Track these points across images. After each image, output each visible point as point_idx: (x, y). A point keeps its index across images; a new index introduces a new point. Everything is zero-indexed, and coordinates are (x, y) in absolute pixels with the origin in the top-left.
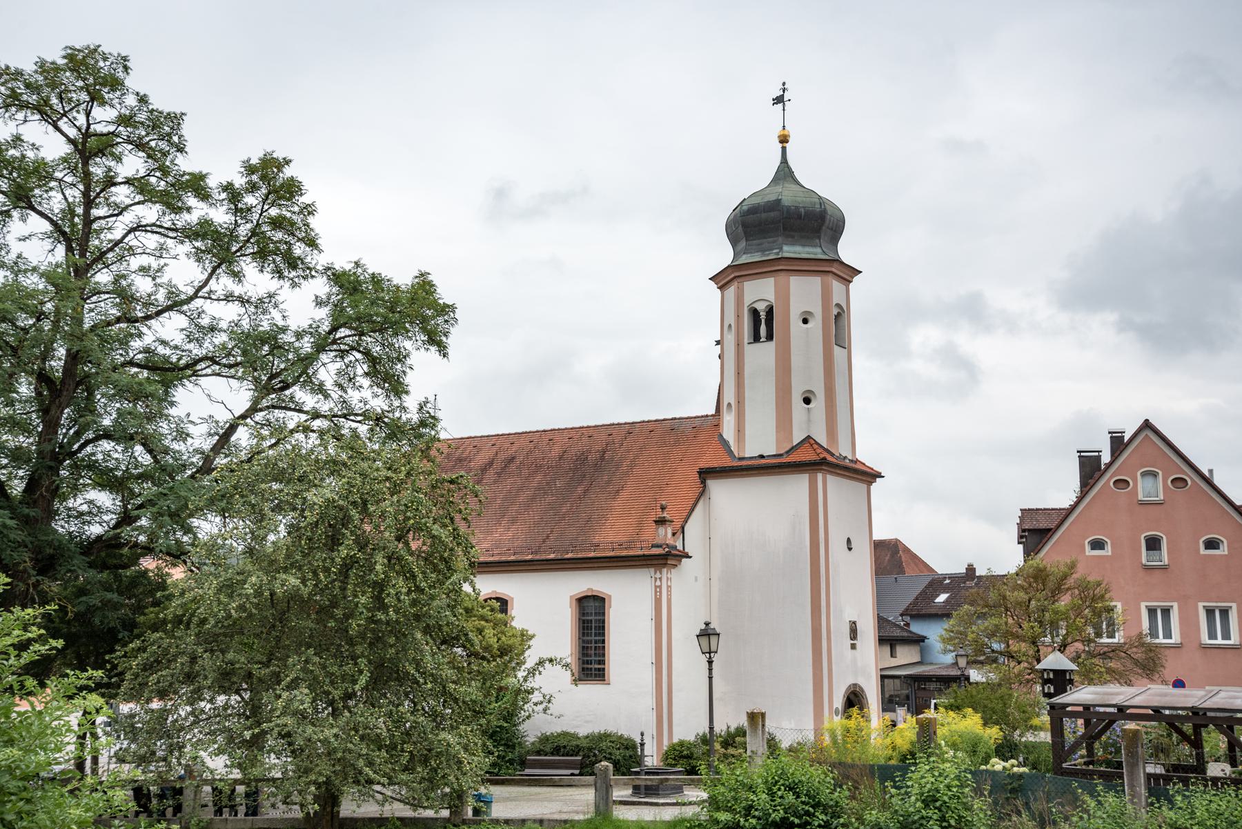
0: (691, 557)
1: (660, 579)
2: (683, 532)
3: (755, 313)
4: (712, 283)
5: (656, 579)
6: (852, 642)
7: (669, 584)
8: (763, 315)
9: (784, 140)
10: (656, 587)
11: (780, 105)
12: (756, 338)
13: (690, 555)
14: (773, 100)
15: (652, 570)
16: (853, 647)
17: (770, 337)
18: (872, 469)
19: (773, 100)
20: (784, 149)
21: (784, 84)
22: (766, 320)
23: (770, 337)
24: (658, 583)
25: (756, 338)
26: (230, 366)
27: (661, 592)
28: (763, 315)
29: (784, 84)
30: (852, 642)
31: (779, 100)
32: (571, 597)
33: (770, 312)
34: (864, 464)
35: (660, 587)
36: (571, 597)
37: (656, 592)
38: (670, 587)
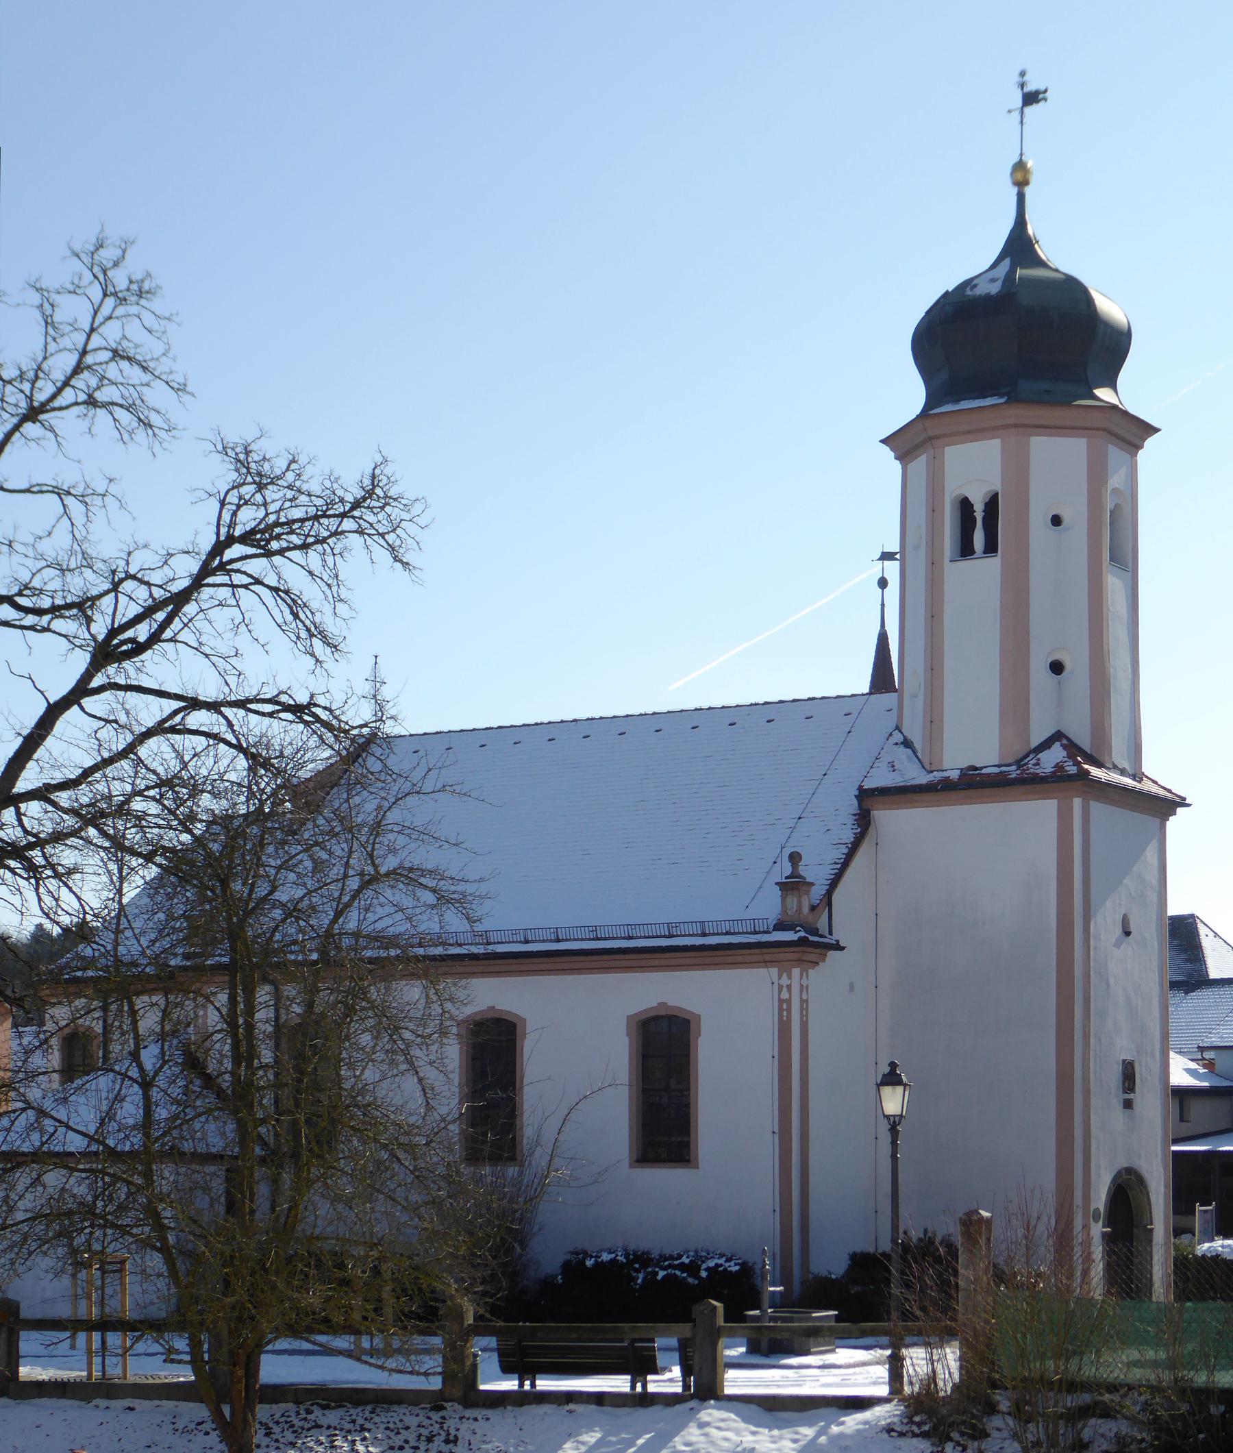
0: (843, 948)
1: (789, 987)
2: (830, 905)
3: (965, 505)
4: (888, 453)
5: (781, 988)
6: (1127, 1096)
7: (804, 997)
8: (979, 515)
9: (1021, 176)
10: (781, 1001)
11: (1030, 88)
12: (966, 550)
13: (842, 944)
14: (1045, 99)
15: (774, 971)
16: (1128, 1104)
17: (991, 547)
18: (1170, 791)
19: (1045, 99)
20: (1021, 198)
21: (1023, 74)
22: (984, 519)
23: (991, 547)
24: (785, 995)
25: (966, 550)
26: (39, 612)
27: (789, 1010)
28: (979, 515)
29: (1023, 74)
30: (1127, 1096)
31: (1031, 98)
32: (629, 1018)
33: (992, 505)
34: (1155, 782)
35: (789, 1001)
36: (629, 1018)
37: (781, 1010)
38: (807, 1001)
